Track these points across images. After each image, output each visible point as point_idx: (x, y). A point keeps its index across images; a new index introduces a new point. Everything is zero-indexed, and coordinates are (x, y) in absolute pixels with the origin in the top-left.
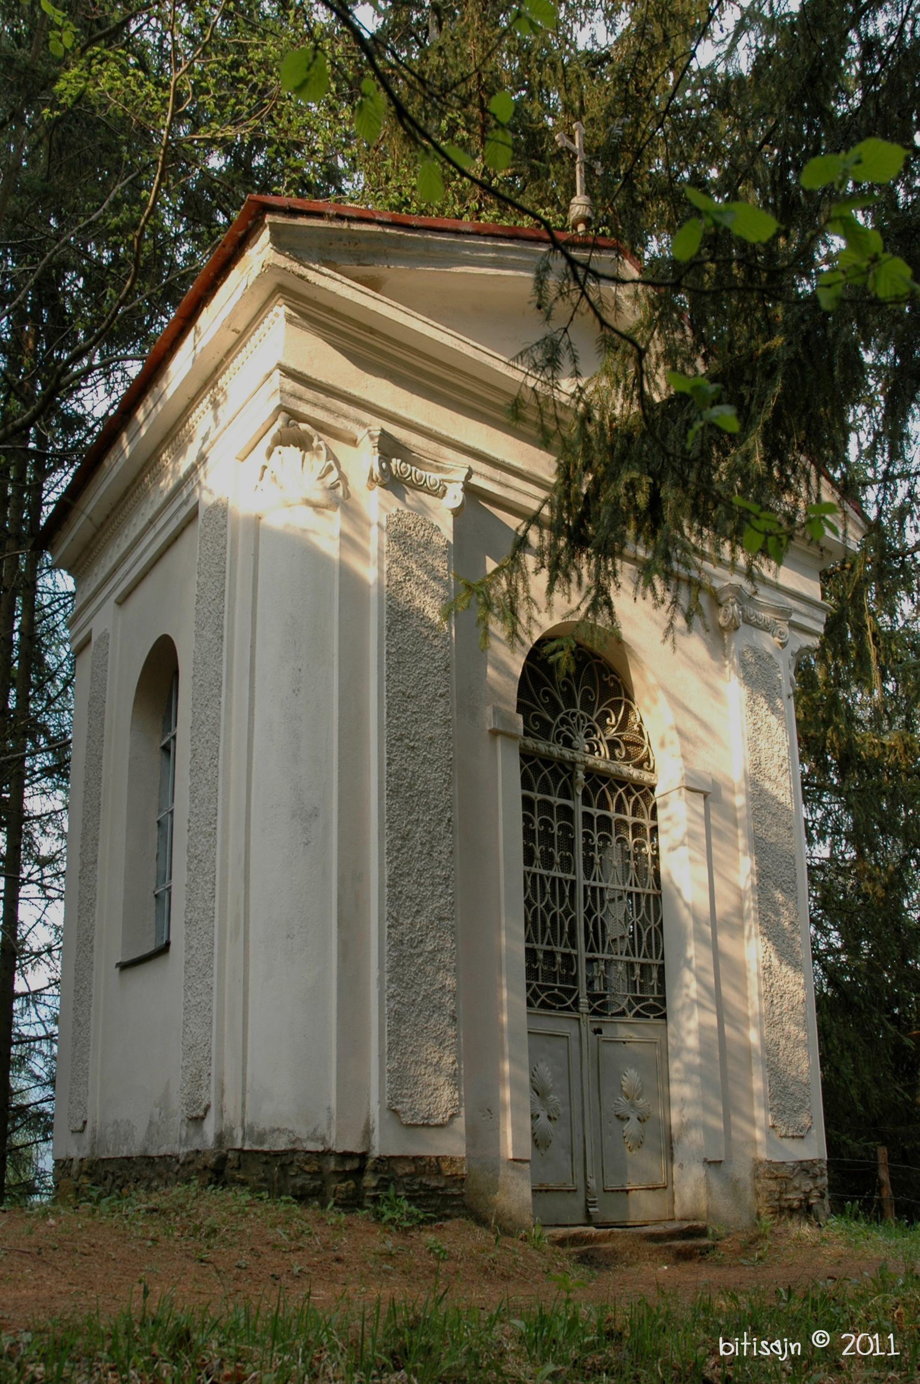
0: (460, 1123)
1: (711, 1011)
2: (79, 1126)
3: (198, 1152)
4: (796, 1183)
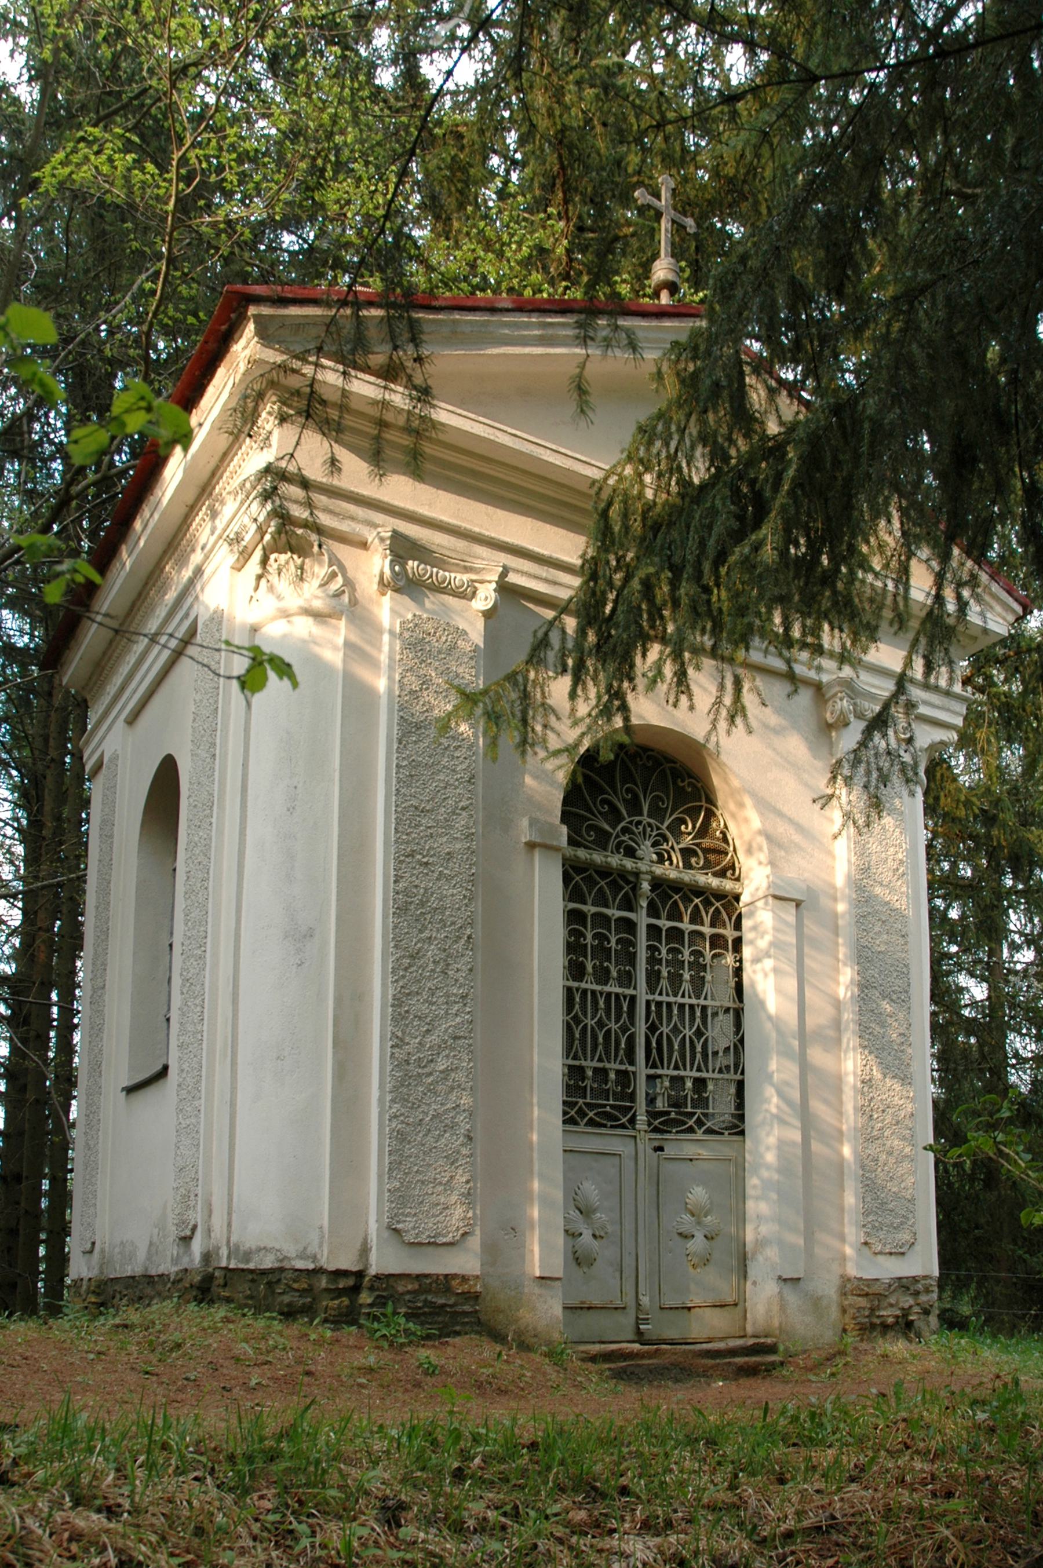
0: (475, 1242)
1: (795, 1127)
2: (88, 1246)
3: (186, 1270)
4: (892, 1300)
